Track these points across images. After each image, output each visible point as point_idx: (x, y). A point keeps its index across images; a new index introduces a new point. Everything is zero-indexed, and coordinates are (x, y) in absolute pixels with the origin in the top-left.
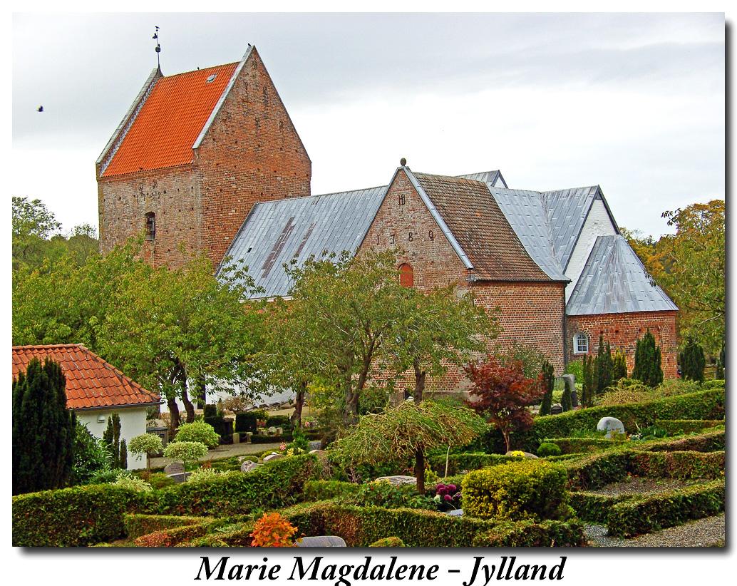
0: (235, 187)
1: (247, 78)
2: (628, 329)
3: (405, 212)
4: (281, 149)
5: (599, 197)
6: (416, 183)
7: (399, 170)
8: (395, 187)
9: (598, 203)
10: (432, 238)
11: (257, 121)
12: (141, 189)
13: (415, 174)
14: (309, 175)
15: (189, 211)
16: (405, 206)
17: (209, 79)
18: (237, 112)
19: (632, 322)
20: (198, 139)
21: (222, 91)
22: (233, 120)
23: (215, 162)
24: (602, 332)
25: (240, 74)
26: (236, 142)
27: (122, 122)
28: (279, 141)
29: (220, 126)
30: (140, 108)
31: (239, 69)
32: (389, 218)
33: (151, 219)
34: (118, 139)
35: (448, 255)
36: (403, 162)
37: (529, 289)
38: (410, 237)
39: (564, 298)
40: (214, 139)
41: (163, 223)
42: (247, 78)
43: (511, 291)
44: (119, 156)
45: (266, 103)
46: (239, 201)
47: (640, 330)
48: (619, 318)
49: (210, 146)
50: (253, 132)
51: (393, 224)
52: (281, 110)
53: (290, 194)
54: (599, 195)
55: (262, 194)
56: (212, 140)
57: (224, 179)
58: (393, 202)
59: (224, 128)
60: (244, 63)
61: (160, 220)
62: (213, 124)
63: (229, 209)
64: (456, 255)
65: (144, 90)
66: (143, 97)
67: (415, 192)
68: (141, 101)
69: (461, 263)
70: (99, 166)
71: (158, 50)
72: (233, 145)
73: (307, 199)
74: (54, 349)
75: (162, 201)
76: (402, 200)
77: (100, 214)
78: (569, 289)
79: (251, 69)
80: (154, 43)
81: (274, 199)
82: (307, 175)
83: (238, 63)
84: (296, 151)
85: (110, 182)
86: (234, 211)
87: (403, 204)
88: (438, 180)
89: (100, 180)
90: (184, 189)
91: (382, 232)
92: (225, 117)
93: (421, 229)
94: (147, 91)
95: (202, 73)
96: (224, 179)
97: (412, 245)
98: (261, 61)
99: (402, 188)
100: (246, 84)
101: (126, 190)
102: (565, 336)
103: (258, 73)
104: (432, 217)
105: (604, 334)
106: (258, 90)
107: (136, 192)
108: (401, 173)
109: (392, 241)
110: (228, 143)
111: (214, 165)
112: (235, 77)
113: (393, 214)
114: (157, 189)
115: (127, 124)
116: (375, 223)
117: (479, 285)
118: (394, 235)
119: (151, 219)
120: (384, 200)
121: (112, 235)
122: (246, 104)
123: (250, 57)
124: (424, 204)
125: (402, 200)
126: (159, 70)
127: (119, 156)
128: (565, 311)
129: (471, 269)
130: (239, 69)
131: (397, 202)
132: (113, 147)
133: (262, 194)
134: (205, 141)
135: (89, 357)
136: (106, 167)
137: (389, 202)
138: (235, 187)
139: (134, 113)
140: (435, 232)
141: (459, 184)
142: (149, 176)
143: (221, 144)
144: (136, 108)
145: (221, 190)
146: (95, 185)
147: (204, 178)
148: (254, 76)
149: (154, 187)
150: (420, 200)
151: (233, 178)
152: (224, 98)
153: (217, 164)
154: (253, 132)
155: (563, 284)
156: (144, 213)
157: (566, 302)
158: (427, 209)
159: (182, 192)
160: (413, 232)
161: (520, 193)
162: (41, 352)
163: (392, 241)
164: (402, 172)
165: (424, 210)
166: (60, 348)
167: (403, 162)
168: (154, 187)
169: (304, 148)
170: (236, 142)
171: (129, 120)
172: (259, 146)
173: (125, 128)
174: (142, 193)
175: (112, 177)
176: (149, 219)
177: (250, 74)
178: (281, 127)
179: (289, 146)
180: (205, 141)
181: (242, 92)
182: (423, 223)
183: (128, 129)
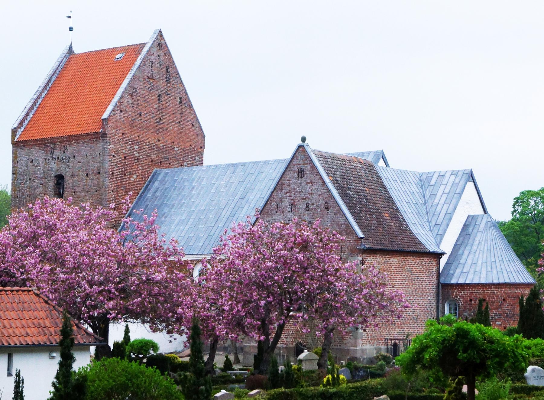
0: (137, 155)
1: (153, 58)
2: (494, 298)
3: (303, 184)
4: (179, 122)
5: (471, 179)
6: (315, 159)
7: (300, 147)
8: (296, 162)
9: (470, 185)
10: (327, 209)
11: (160, 96)
12: (52, 153)
13: (313, 151)
14: (202, 148)
15: (95, 175)
16: (304, 179)
17: (118, 56)
18: (142, 87)
19: (497, 292)
20: (107, 110)
21: (130, 68)
22: (138, 95)
23: (121, 132)
24: (471, 300)
25: (147, 54)
26: (140, 115)
27: (36, 92)
28: (178, 115)
29: (128, 100)
30: (52, 81)
31: (146, 49)
32: (288, 189)
33: (61, 181)
34: (32, 107)
35: (341, 225)
36: (304, 139)
37: (410, 259)
38: (307, 207)
39: (439, 268)
40: (121, 111)
41: (71, 185)
42: (153, 58)
43: (395, 260)
44: (33, 123)
45: (168, 81)
46: (140, 168)
47: (504, 300)
48: (486, 288)
49: (117, 117)
50: (156, 106)
51: (292, 195)
52: (181, 88)
53: (185, 164)
54: (471, 177)
55: (161, 162)
56: (119, 112)
57: (128, 147)
58: (293, 175)
59: (130, 102)
60: (151, 43)
61: (69, 182)
62: (121, 98)
63: (131, 174)
64: (348, 225)
65: (57, 64)
66: (56, 71)
67: (313, 166)
68: (53, 74)
69: (352, 232)
70: (14, 132)
71: (71, 29)
72: (138, 117)
73: (199, 167)
74: (12, 291)
75: (71, 165)
76: (301, 173)
77: (13, 174)
78: (444, 261)
79: (156, 49)
80: (68, 23)
81: (171, 167)
82: (201, 148)
83: (144, 45)
84: (193, 125)
85: (24, 146)
86: (135, 177)
87: (302, 177)
88: (334, 158)
89: (16, 144)
90: (91, 155)
91: (281, 201)
92: (132, 92)
93: (318, 201)
94: (59, 66)
95: (113, 51)
96: (128, 147)
97: (308, 214)
98: (165, 43)
99: (302, 162)
100: (152, 63)
101: (39, 155)
102: (438, 303)
103: (162, 54)
104: (329, 191)
105: (473, 302)
106: (162, 69)
107: (47, 155)
108: (301, 149)
109: (289, 210)
110: (133, 115)
111: (120, 134)
112: (142, 56)
113: (292, 186)
114: (67, 154)
115: (41, 94)
116: (275, 193)
117: (368, 253)
118: (292, 205)
119: (61, 181)
120: (284, 172)
121: (23, 194)
122: (151, 81)
123: (156, 39)
124: (321, 178)
125: (301, 173)
126: (71, 47)
127: (33, 123)
128: (439, 280)
129: (362, 238)
130: (146, 49)
131: (296, 175)
132: (28, 114)
133: (161, 162)
134: (114, 113)
135: (42, 301)
136: (20, 132)
137: (289, 175)
138: (137, 155)
139: (47, 84)
140: (331, 204)
141: (343, 160)
142: (60, 142)
143: (126, 115)
144: (49, 81)
145: (125, 158)
146: (10, 148)
147: (111, 146)
148: (159, 56)
149: (64, 152)
150: (318, 174)
151: (136, 147)
152: (132, 74)
153: (123, 134)
154: (156, 106)
155: (438, 256)
156: (53, 175)
157: (441, 271)
158: (324, 183)
159: (90, 157)
160: (310, 202)
161: (400, 173)
162: (19, 293)
163: (289, 210)
164: (301, 150)
165: (321, 183)
166: (17, 291)
167: (304, 139)
168: (64, 152)
169: (199, 123)
170: (140, 115)
171: (43, 91)
172: (160, 119)
173: (38, 97)
174: (52, 157)
175: (26, 141)
176: (57, 181)
177: (156, 54)
178: (180, 103)
179: (186, 120)
180: (114, 113)
181: (147, 69)
182: (320, 195)
183: (41, 99)
